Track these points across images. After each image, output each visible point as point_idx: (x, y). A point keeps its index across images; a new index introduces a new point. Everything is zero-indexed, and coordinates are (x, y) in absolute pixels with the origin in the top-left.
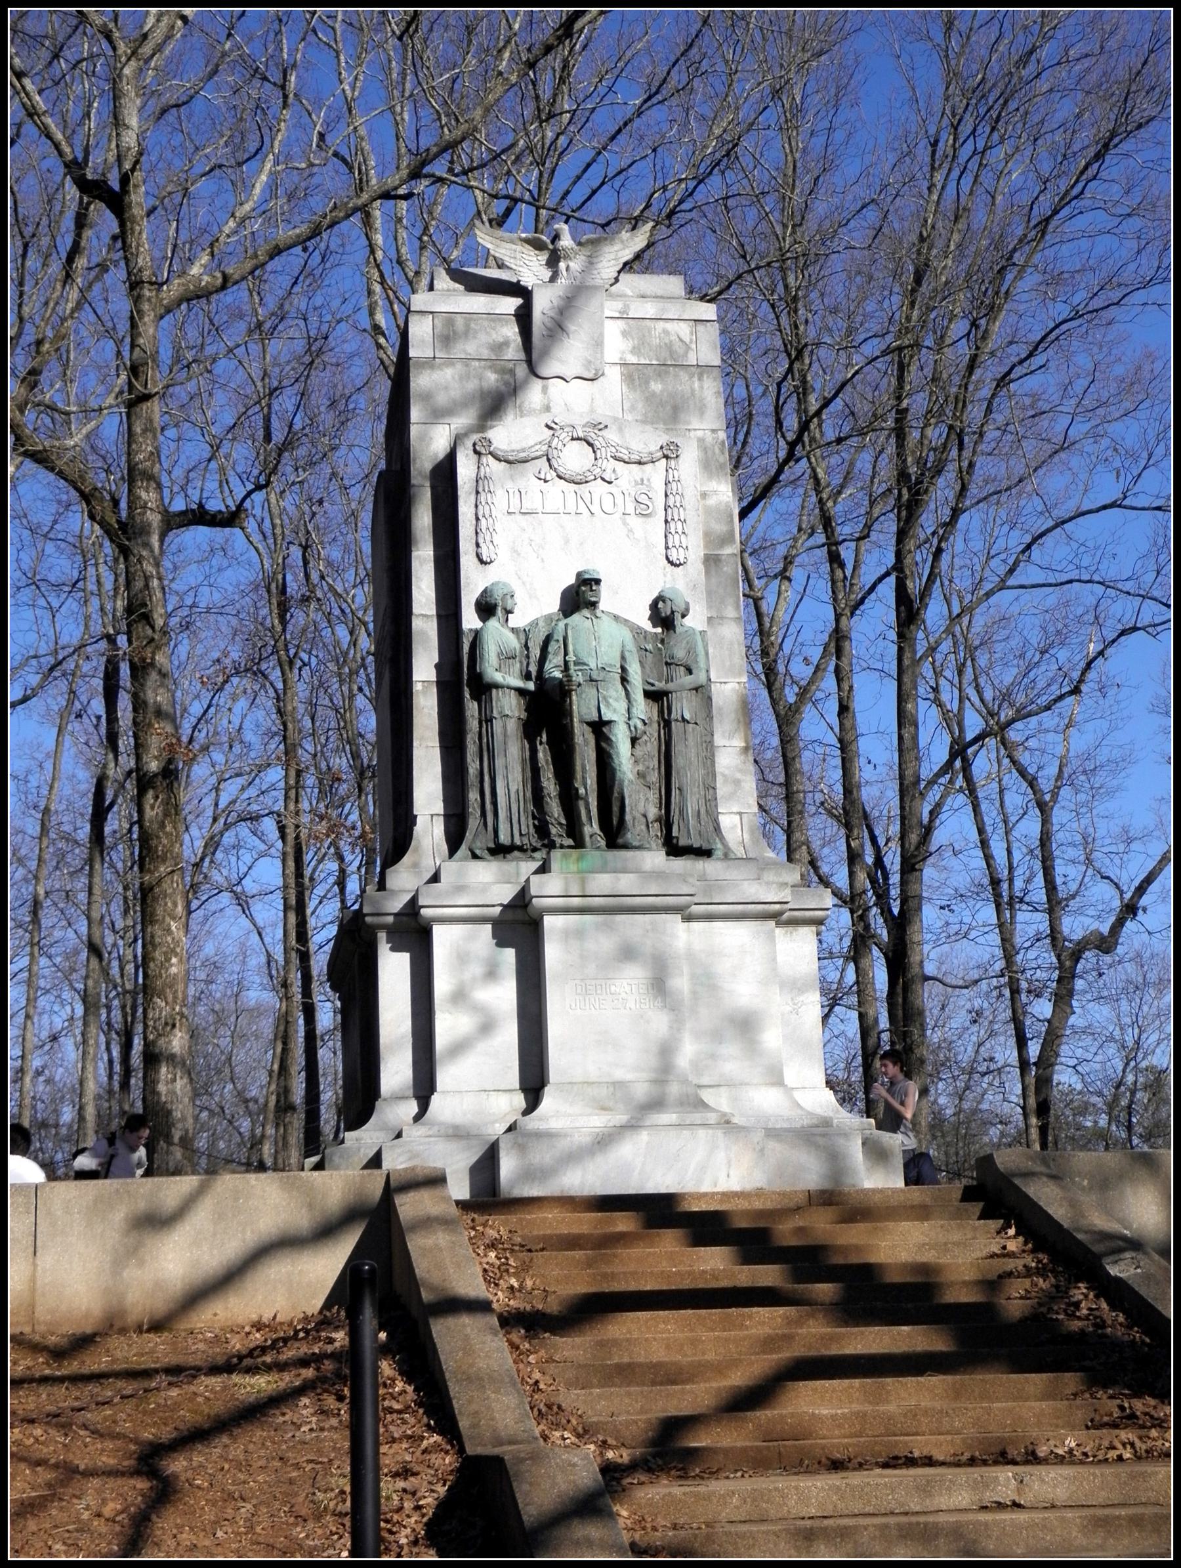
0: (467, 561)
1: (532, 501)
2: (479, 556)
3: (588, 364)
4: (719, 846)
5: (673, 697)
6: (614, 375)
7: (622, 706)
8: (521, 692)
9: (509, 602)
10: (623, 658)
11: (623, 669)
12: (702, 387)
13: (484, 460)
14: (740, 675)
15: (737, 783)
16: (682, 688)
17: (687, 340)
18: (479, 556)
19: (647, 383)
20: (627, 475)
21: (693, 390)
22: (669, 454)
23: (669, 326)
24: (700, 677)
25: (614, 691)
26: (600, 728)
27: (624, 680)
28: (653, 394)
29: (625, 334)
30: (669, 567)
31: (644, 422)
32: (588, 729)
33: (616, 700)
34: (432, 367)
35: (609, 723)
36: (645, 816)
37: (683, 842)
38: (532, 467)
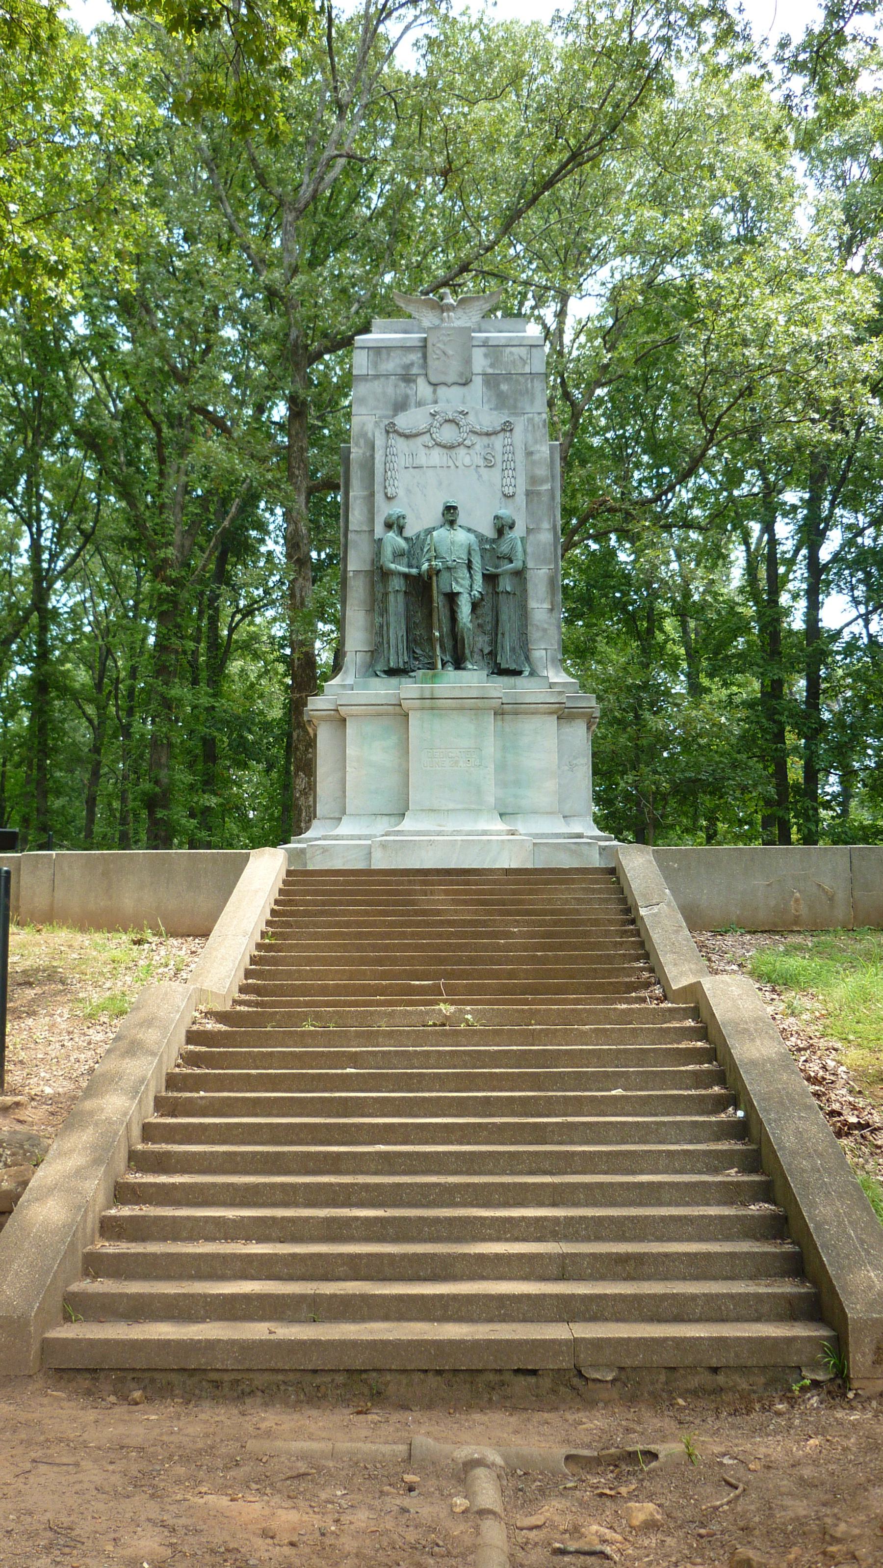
0: (379, 497)
1: (422, 460)
2: (386, 494)
3: (461, 374)
4: (528, 669)
5: (501, 579)
6: (478, 381)
7: (467, 583)
8: (406, 576)
9: (402, 521)
10: (469, 554)
11: (470, 561)
12: (533, 387)
13: (391, 435)
14: (550, 564)
15: (545, 630)
16: (505, 572)
17: (525, 358)
18: (386, 494)
19: (498, 385)
20: (480, 443)
21: (527, 389)
22: (507, 428)
23: (513, 349)
24: (517, 564)
25: (463, 573)
26: (452, 598)
27: (469, 566)
28: (502, 392)
29: (486, 356)
30: (510, 500)
31: (495, 409)
32: (441, 597)
33: (463, 579)
34: (366, 380)
35: (458, 594)
36: (481, 650)
37: (504, 666)
38: (420, 440)
